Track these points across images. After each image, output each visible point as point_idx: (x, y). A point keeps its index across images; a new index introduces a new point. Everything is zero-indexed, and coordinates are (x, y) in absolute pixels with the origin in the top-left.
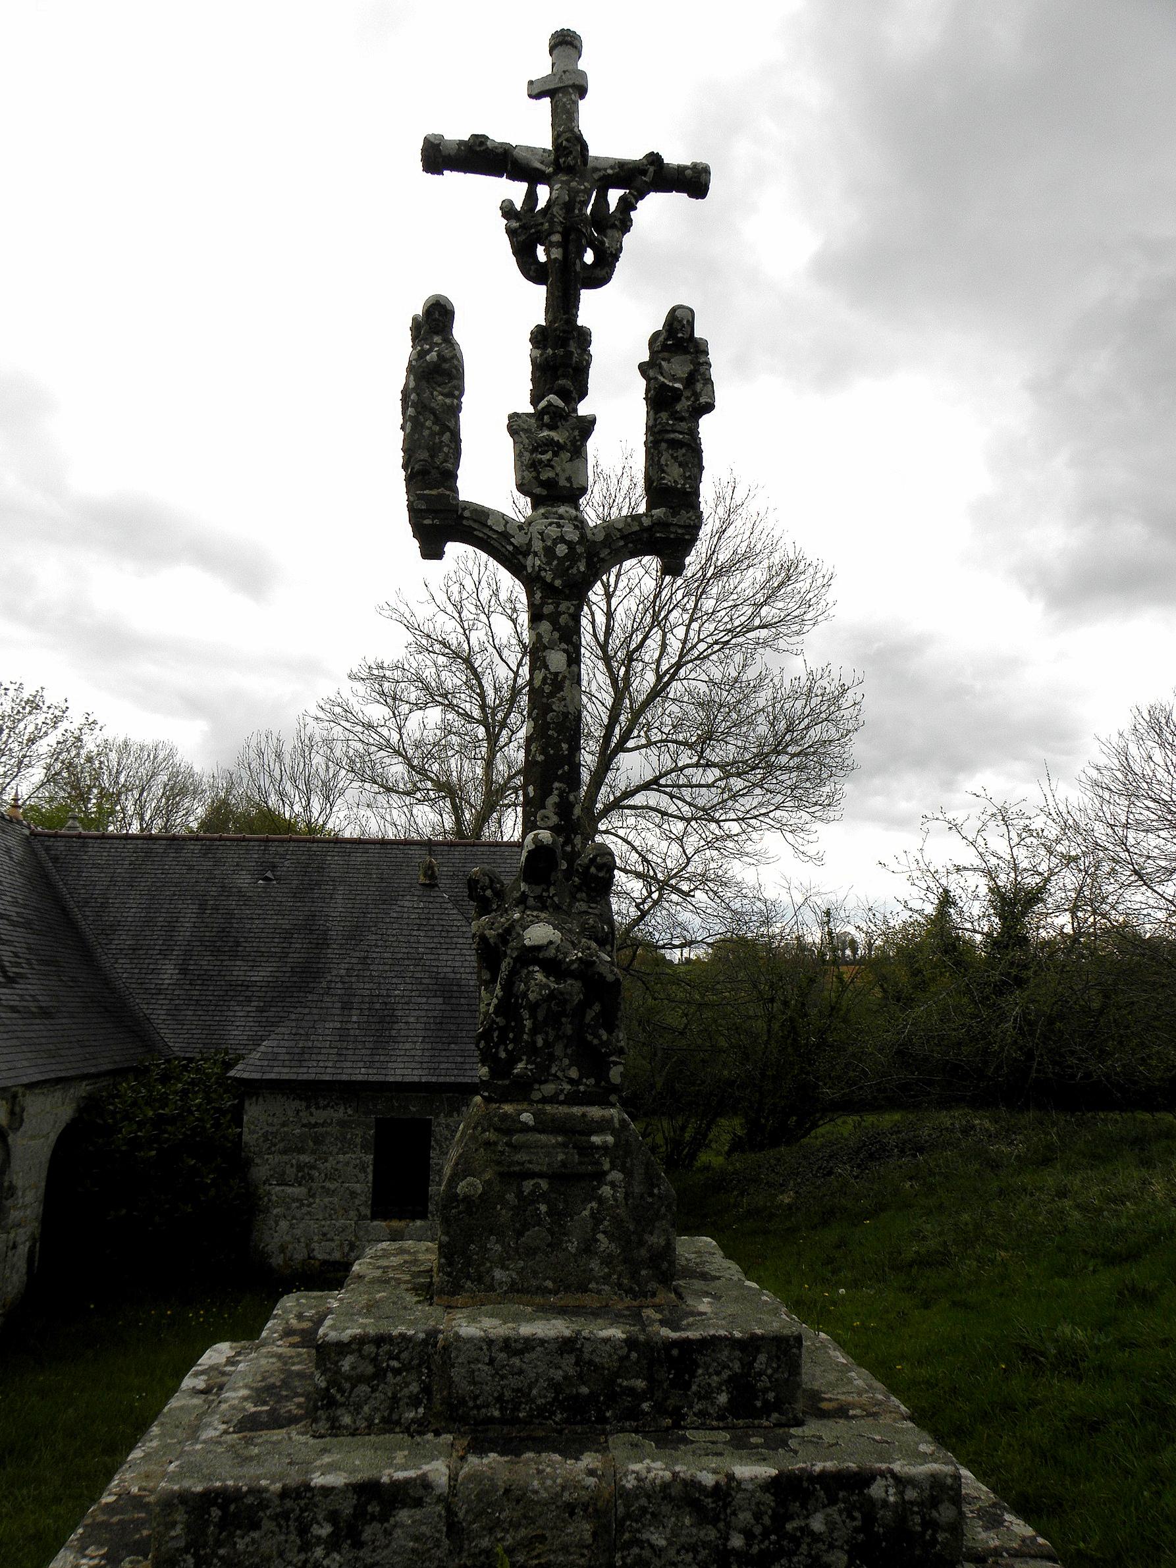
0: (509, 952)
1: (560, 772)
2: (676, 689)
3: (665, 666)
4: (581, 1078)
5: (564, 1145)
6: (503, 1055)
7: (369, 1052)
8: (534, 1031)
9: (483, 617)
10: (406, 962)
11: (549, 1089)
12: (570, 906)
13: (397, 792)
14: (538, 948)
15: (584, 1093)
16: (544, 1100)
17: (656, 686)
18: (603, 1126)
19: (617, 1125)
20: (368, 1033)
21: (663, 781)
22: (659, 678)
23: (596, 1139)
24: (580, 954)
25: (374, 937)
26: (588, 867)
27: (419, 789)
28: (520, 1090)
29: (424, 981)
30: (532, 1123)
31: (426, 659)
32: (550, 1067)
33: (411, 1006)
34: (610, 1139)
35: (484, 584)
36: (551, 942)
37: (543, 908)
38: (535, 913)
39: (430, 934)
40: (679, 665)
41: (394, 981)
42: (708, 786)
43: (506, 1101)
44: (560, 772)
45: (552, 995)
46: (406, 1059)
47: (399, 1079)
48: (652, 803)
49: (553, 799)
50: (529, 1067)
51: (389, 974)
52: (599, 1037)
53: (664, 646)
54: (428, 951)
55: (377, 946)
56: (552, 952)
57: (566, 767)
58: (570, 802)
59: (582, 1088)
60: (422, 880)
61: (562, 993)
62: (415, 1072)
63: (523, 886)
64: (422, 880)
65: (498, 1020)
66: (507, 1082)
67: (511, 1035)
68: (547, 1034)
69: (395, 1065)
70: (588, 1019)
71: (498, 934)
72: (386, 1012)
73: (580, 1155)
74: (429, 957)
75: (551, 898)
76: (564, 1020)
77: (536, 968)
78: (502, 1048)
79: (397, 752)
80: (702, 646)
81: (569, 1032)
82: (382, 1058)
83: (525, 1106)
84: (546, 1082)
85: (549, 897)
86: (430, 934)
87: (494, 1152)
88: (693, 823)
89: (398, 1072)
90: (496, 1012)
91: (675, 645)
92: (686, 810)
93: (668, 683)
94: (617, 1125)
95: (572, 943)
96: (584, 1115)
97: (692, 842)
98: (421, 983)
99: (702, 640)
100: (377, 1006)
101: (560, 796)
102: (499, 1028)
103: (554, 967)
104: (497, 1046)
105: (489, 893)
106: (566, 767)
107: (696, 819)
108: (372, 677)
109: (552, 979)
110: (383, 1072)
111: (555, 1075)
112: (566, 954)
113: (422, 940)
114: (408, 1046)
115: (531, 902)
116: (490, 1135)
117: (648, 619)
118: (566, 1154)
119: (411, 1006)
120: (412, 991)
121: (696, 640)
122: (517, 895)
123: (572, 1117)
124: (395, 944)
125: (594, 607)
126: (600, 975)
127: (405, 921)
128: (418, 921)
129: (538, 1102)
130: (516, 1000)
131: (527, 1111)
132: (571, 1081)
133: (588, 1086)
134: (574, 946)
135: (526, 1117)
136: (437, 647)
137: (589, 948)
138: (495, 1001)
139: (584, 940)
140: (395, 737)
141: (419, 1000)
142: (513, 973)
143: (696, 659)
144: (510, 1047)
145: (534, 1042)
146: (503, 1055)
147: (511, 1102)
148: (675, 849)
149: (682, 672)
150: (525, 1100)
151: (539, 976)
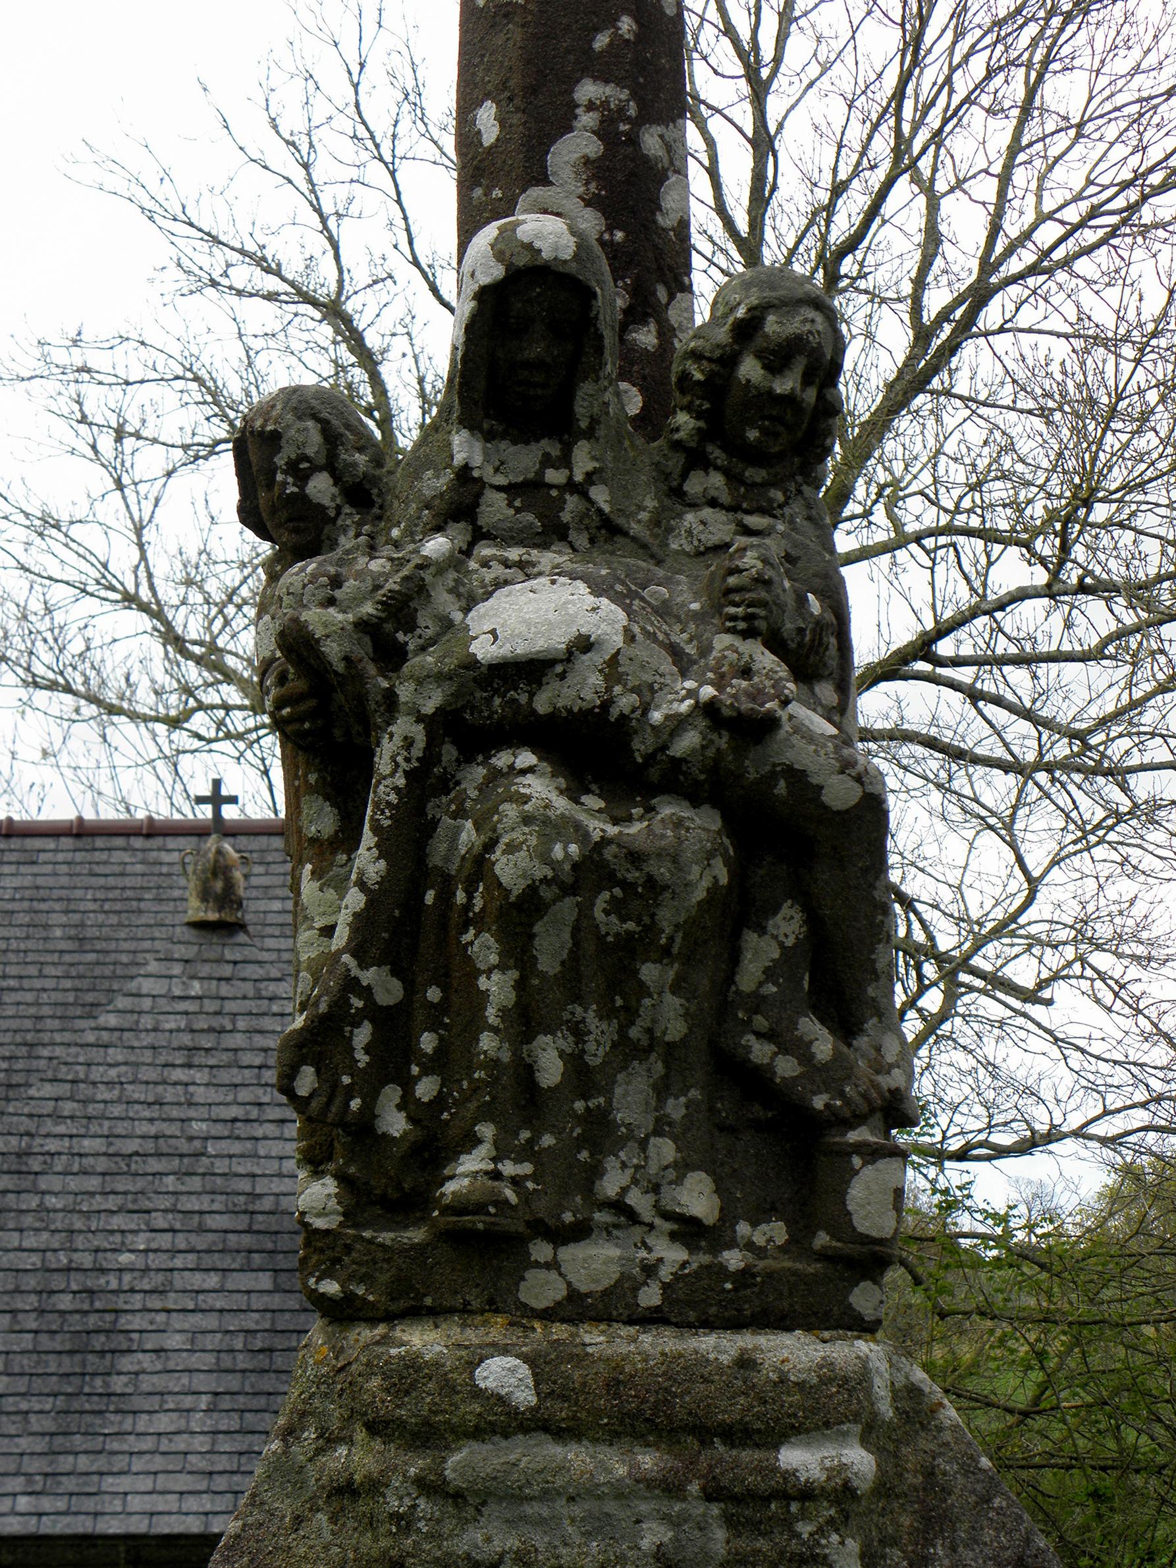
0: (405, 692)
1: (601, 41)
2: (975, 366)
3: (936, 300)
4: (728, 1217)
5: (668, 1487)
6: (395, 1123)
7: (40, 1445)
8: (525, 1021)
9: (377, 174)
10: (154, 1165)
11: (595, 1262)
12: (661, 523)
13: (133, 716)
14: (531, 670)
15: (744, 1276)
16: (577, 1308)
17: (911, 359)
18: (827, 1406)
19: (886, 1409)
20: (38, 1384)
21: (945, 648)
22: (922, 334)
23: (801, 1459)
24: (708, 691)
25: (48, 1090)
26: (728, 361)
27: (201, 707)
28: (482, 1260)
29: (212, 1222)
30: (525, 1397)
31: (210, 308)
32: (595, 1171)
33: (172, 1301)
34: (859, 1460)
35: (374, 75)
36: (584, 644)
37: (552, 533)
38: (514, 554)
39: (225, 1076)
40: (980, 295)
41: (117, 1222)
42: (1083, 657)
43: (415, 1313)
44: (601, 41)
45: (593, 870)
46: (158, 1463)
47: (138, 1526)
48: (916, 721)
49: (576, 147)
50: (508, 1168)
51: (98, 1202)
52: (801, 1050)
53: (932, 240)
54: (219, 1130)
55: (58, 1117)
56: (585, 686)
57: (626, 25)
58: (646, 161)
59: (733, 1259)
60: (196, 910)
61: (635, 857)
62: (191, 1504)
63: (463, 447)
64: (196, 910)
65: (368, 977)
66: (417, 1235)
67: (428, 1042)
68: (578, 1032)
69: (124, 1483)
70: (750, 975)
71: (362, 625)
72: (93, 1321)
73: (730, 1521)
74: (225, 1146)
75: (580, 489)
76: (649, 972)
77: (526, 758)
78: (391, 1094)
79: (130, 600)
80: (1048, 233)
81: (675, 1029)
82: (83, 1463)
83: (497, 1330)
84: (580, 1232)
85: (571, 486)
86: (225, 1076)
87: (371, 1523)
88: (1042, 777)
89: (135, 1503)
90: (359, 949)
91: (965, 224)
92: (1023, 738)
93: (952, 348)
94: (886, 1409)
95: (675, 652)
96: (745, 1362)
97: (1041, 831)
98: (202, 1230)
99: (1050, 216)
100: (65, 1302)
101: (605, 132)
102: (375, 1013)
103: (596, 750)
104: (371, 1088)
105: (321, 487)
106: (626, 25)
107: (1049, 768)
108: (48, 370)
109: (593, 802)
110: (89, 1504)
111: (619, 1206)
112: (648, 694)
113: (200, 1094)
114: (164, 1422)
115: (495, 508)
116: (357, 1457)
117: (882, 146)
118: (674, 1522)
119: (172, 1301)
120: (174, 1252)
121: (1030, 217)
122: (436, 483)
123: (696, 1370)
124: (117, 1110)
125: (715, 125)
126: (796, 776)
127: (147, 1039)
128: (186, 1039)
129: (548, 1315)
130: (446, 896)
131: (505, 1351)
132: (689, 1231)
133: (758, 1251)
134: (683, 664)
135: (504, 1375)
136: (244, 275)
137: (746, 672)
138: (355, 899)
139: (722, 641)
140: (123, 560)
141: (197, 1280)
142: (427, 782)
143: (1033, 270)
144: (426, 1089)
145: (526, 1071)
146: (395, 1123)
147: (434, 1314)
148: (992, 852)
149: (991, 315)
150: (493, 1306)
151: (541, 788)
